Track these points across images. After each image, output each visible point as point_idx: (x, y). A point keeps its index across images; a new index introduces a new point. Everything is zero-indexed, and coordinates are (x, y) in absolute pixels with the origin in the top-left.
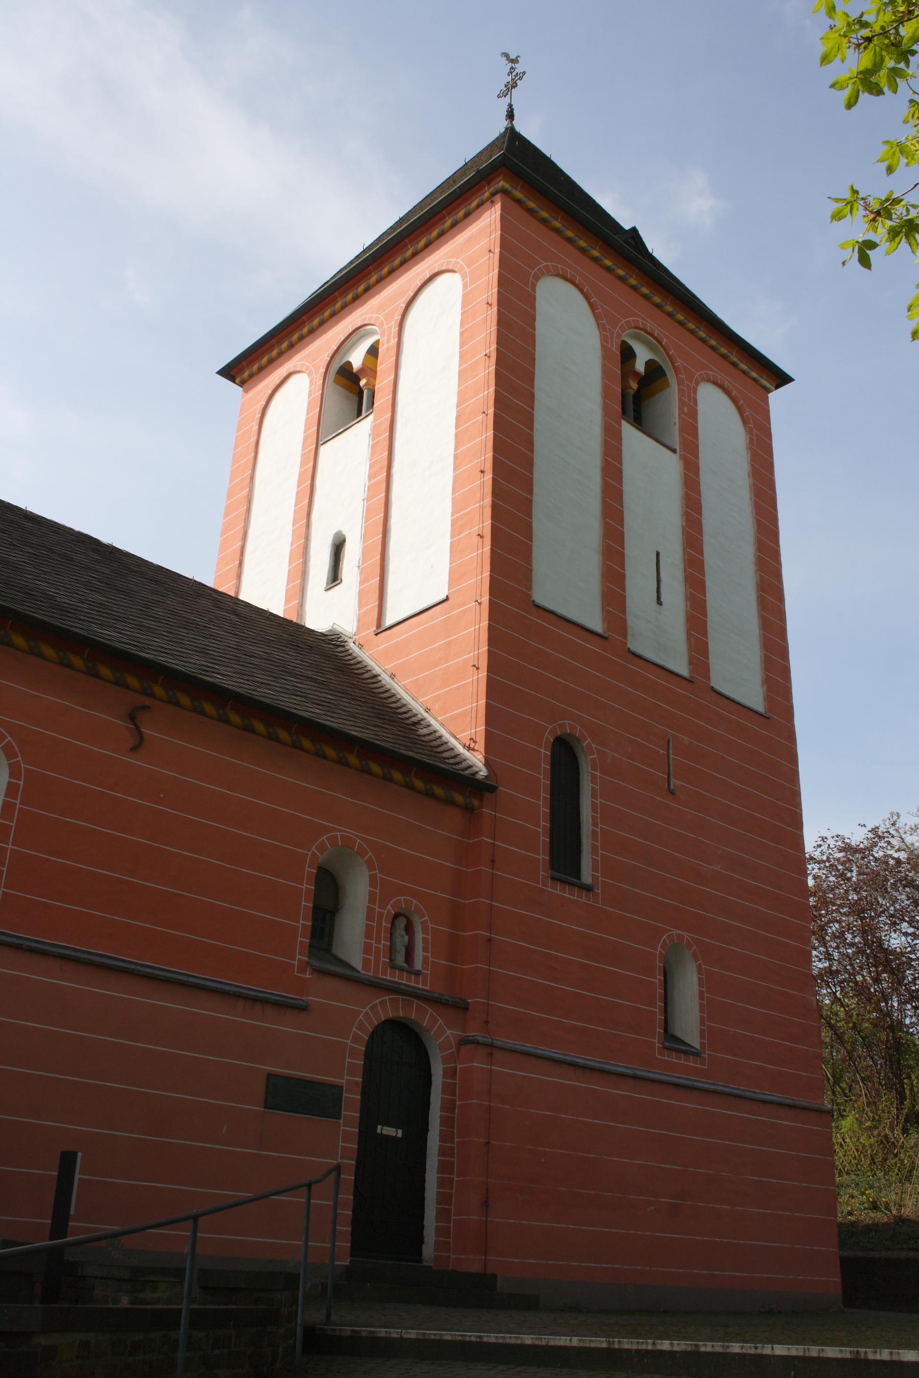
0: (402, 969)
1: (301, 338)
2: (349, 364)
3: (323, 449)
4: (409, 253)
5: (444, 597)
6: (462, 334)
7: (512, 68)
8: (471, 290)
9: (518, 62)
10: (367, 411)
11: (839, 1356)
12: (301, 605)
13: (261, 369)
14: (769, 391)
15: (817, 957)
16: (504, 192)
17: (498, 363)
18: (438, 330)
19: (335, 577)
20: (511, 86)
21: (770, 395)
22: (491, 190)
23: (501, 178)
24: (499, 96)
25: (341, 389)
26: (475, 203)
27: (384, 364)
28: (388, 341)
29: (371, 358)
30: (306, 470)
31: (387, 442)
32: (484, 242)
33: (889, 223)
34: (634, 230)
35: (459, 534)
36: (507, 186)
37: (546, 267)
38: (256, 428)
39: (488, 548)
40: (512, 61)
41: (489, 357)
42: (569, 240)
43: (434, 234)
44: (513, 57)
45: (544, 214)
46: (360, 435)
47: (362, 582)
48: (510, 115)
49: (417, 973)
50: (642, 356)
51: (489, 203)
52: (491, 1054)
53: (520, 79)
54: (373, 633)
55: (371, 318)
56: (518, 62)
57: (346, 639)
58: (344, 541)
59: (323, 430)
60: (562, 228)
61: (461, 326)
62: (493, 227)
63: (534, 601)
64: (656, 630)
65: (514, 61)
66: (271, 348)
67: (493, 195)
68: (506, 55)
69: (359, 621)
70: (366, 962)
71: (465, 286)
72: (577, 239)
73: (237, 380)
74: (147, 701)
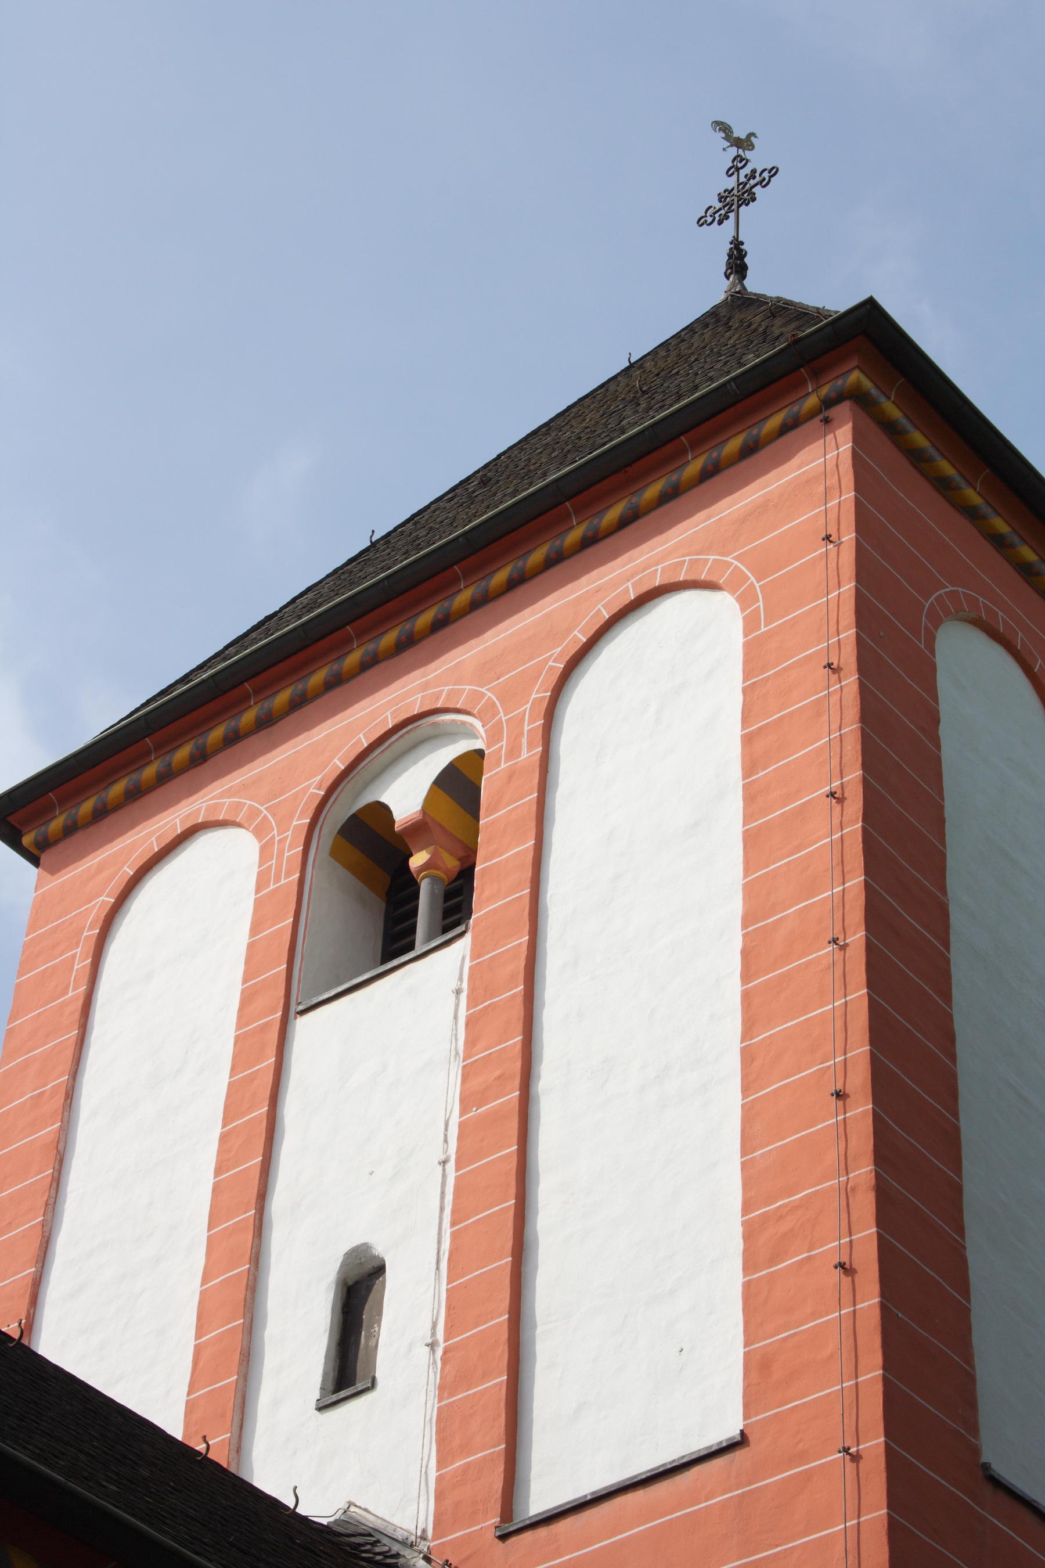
1: (233, 739)
2: (382, 811)
3: (304, 1027)
4: (575, 535)
5: (730, 1428)
6: (747, 740)
7: (737, 157)
8: (769, 635)
9: (751, 147)
10: (430, 938)
13: (101, 814)
16: (859, 398)
17: (869, 815)
18: (665, 735)
19: (359, 1289)
20: (736, 200)
22: (824, 391)
23: (854, 363)
24: (701, 222)
25: (342, 871)
26: (775, 421)
27: (500, 811)
28: (513, 751)
29: (446, 803)
30: (251, 1079)
31: (518, 1011)
32: (809, 517)
35: (773, 1261)
36: (867, 384)
38: (82, 964)
39: (870, 1302)
40: (738, 143)
41: (841, 800)
42: (998, 542)
43: (652, 491)
44: (740, 133)
45: (947, 468)
46: (433, 987)
47: (444, 1389)
48: (737, 264)
53: (764, 184)
54: (491, 1534)
55: (454, 694)
56: (751, 147)
57: (396, 1548)
58: (379, 1270)
59: (294, 984)
60: (986, 509)
61: (746, 720)
62: (833, 481)
63: (986, 1467)
65: (744, 143)
66: (142, 759)
67: (828, 403)
68: (724, 128)
69: (439, 1496)
71: (750, 624)
72: (1016, 540)
73: (27, 840)
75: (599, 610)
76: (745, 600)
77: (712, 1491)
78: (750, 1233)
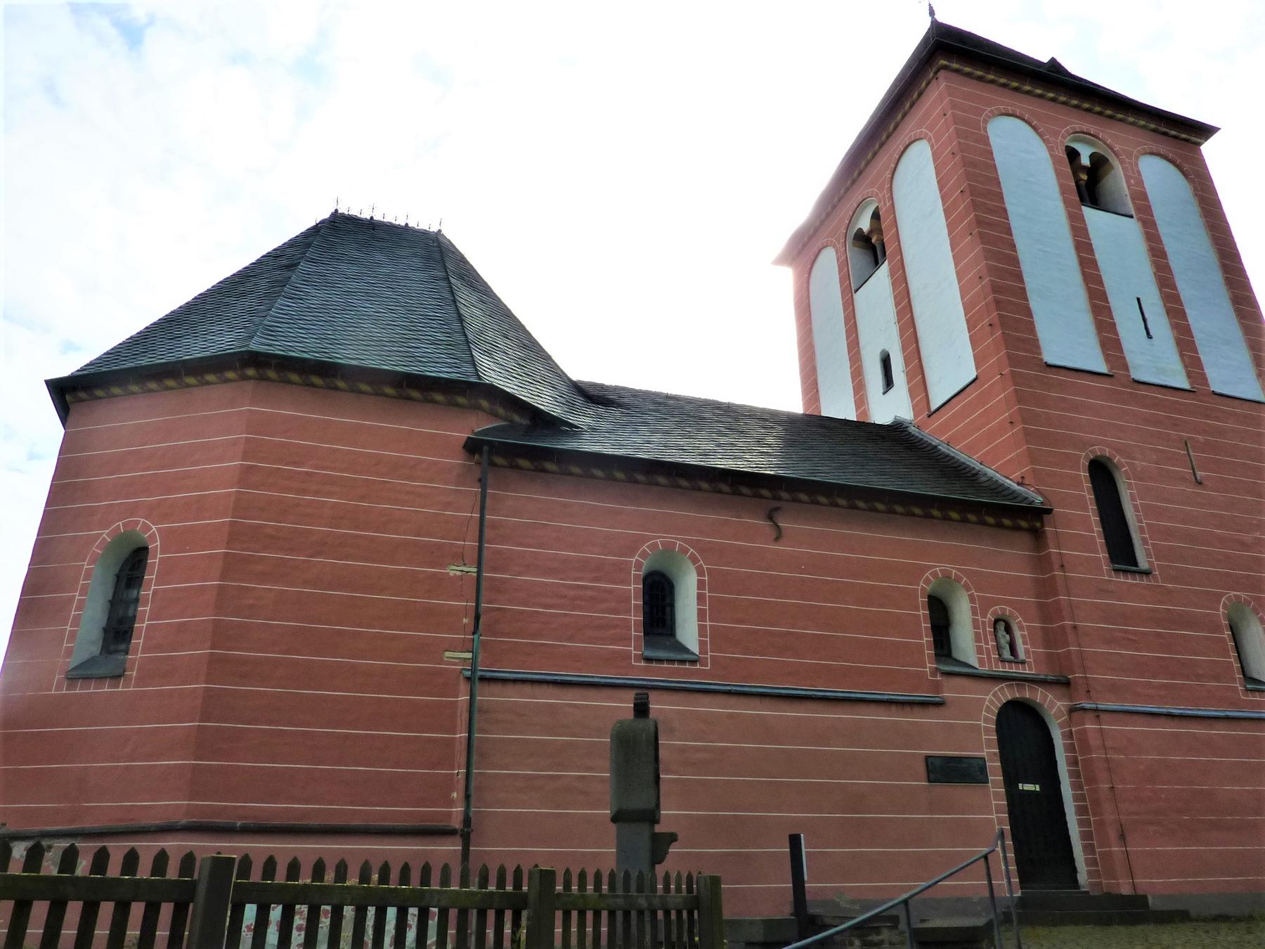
0: (1010, 662)
3: (859, 297)
14: (1200, 144)
19: (886, 362)
21: (1209, 149)
34: (1053, 60)
37: (991, 112)
42: (1004, 86)
45: (979, 73)
49: (1023, 662)
52: (1098, 717)
64: (1156, 360)
67: (936, 73)
70: (981, 661)
71: (932, 147)
74: (776, 504)
75: (144, 651)
76: (929, 140)
77: (973, 394)
78: (968, 322)
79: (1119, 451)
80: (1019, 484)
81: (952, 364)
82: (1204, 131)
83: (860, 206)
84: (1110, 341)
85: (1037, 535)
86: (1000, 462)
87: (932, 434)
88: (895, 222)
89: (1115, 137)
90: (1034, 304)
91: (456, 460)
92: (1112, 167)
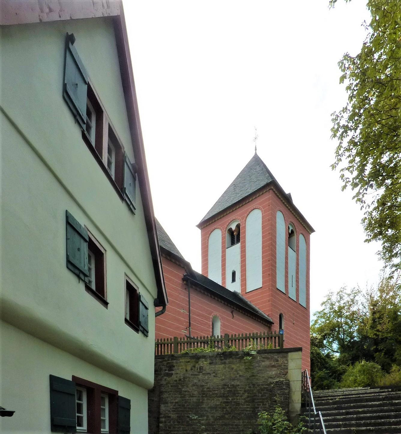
11: (107, 168)
12: (207, 272)
15: (277, 420)
19: (234, 274)
21: (310, 235)
25: (229, 235)
33: (350, 183)
34: (290, 195)
50: (291, 228)
51: (268, 192)
67: (269, 190)
74: (233, 310)
77: (260, 291)
79: (284, 313)
80: (267, 316)
81: (255, 281)
82: (312, 230)
83: (233, 221)
84: (286, 287)
85: (270, 328)
86: (264, 310)
87: (247, 299)
88: (245, 232)
89: (299, 228)
90: (277, 271)
91: (180, 282)
92: (294, 236)
